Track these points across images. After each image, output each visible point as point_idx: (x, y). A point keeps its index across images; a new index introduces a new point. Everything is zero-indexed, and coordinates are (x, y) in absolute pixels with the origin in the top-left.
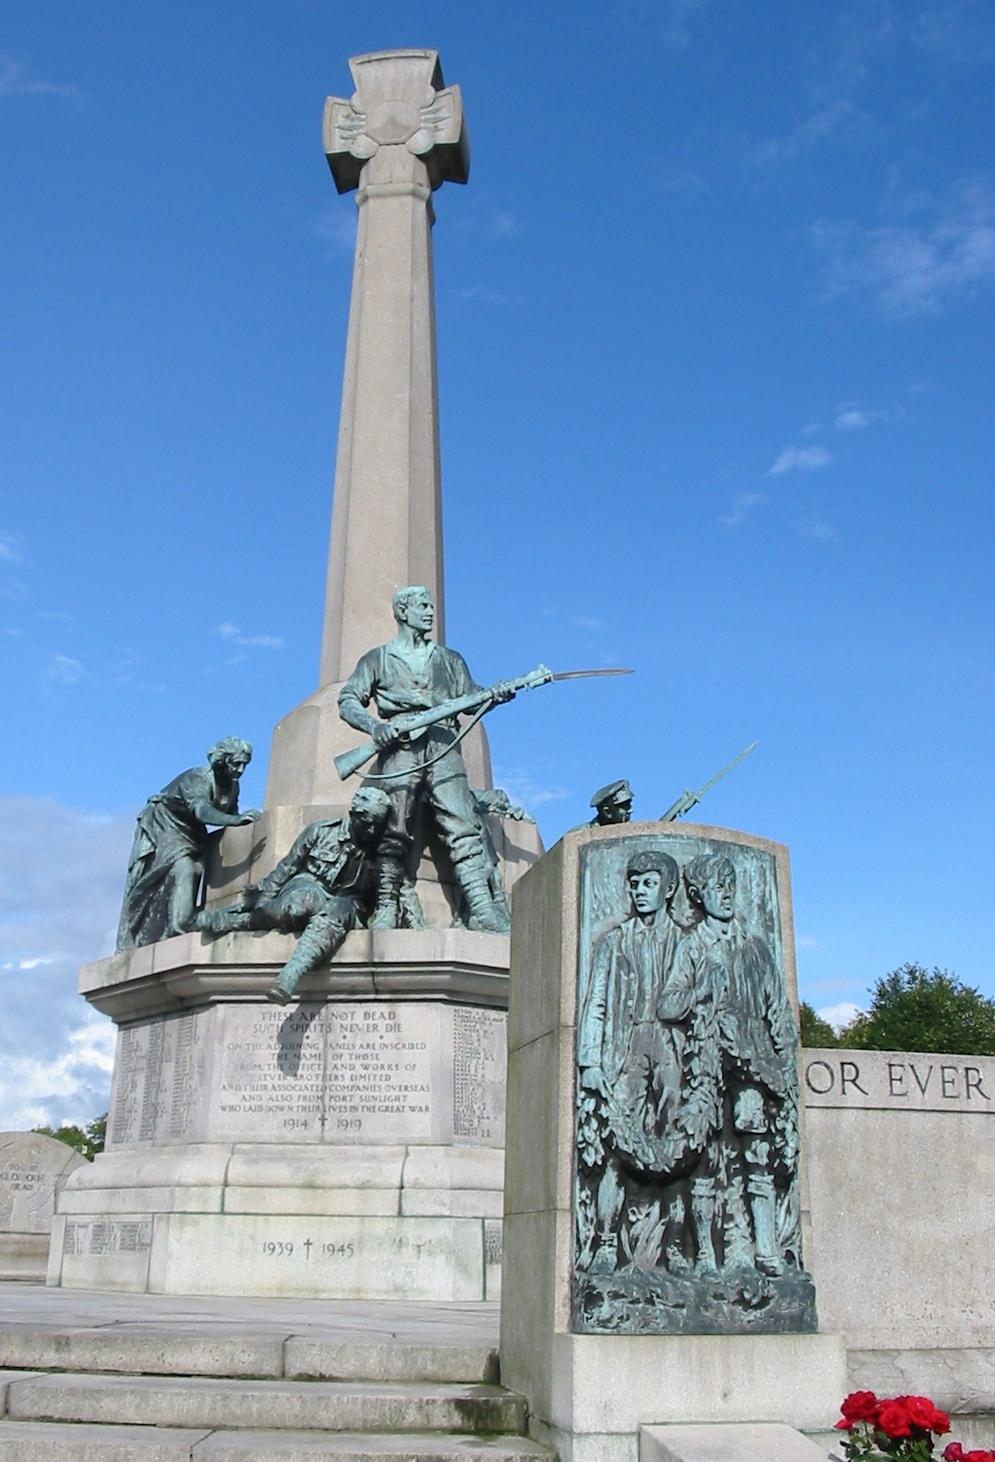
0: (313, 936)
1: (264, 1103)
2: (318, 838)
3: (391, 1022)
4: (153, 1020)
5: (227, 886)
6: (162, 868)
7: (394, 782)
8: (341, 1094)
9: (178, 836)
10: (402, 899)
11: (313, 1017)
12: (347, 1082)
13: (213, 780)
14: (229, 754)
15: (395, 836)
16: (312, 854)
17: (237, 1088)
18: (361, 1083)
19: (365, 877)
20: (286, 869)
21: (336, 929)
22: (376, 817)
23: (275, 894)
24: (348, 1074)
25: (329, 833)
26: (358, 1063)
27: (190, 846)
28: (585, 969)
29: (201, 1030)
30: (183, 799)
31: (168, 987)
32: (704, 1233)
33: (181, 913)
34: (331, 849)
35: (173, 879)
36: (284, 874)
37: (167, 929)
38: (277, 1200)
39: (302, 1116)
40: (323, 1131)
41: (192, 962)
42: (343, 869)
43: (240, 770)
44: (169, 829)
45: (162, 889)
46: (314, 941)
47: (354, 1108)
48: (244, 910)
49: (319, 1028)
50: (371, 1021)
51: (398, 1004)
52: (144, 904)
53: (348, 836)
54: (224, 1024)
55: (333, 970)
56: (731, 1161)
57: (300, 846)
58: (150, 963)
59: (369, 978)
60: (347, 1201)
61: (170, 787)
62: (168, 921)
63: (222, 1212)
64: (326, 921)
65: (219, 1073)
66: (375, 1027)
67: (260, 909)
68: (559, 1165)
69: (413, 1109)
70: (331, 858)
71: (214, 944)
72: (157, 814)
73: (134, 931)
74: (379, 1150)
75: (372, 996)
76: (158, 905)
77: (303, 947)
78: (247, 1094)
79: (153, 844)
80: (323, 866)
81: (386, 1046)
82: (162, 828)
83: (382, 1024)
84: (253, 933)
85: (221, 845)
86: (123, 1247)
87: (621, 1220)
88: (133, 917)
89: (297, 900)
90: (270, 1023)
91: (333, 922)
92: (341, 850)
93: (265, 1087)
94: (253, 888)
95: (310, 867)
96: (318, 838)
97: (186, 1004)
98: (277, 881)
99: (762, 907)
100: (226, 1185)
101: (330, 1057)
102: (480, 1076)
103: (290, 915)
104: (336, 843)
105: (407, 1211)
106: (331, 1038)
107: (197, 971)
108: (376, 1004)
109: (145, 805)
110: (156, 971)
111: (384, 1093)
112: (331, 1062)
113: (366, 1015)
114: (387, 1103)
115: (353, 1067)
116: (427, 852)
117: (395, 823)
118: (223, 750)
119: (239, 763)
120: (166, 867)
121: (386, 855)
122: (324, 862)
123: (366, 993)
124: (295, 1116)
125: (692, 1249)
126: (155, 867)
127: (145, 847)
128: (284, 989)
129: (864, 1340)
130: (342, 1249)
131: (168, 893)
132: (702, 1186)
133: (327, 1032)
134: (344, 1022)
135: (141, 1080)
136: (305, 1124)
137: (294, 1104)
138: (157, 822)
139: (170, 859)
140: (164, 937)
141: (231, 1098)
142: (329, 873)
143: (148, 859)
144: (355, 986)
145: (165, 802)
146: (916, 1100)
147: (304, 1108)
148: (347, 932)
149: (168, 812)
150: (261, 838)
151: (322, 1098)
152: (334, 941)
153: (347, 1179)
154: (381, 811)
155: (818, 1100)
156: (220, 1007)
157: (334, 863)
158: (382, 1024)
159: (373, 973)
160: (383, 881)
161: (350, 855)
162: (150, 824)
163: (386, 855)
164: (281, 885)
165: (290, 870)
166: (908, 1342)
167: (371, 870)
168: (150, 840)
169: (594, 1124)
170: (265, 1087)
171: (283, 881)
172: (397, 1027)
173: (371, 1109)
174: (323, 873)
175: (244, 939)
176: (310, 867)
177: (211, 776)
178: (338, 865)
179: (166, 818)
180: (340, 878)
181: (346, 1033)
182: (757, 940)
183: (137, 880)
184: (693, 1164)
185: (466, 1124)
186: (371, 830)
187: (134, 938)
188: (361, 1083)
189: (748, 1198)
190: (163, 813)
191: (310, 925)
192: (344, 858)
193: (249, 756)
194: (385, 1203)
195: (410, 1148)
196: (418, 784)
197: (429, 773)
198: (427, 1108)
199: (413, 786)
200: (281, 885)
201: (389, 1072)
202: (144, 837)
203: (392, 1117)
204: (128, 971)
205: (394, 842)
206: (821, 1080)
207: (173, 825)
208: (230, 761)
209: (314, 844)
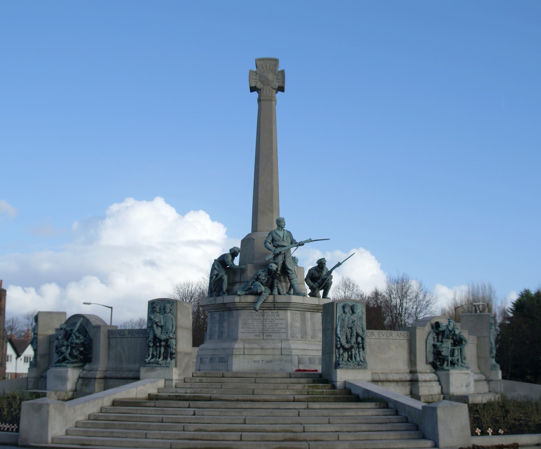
1: (250, 331)
8: (267, 329)
10: (278, 287)
12: (268, 327)
17: (244, 328)
18: (271, 327)
24: (268, 325)
26: (270, 323)
28: (337, 320)
32: (353, 356)
38: (255, 352)
39: (259, 334)
40: (263, 337)
47: (270, 332)
50: (273, 314)
56: (357, 347)
60: (270, 352)
63: (244, 354)
65: (240, 326)
66: (274, 315)
68: (130, 328)
69: (282, 333)
70: (264, 278)
74: (276, 341)
78: (246, 329)
81: (276, 319)
86: (219, 362)
87: (342, 355)
92: (266, 277)
93: (250, 328)
95: (259, 280)
97: (230, 309)
99: (362, 311)
100: (244, 349)
101: (264, 322)
102: (295, 325)
105: (283, 354)
106: (264, 317)
111: (276, 329)
112: (264, 323)
113: (272, 313)
114: (277, 331)
115: (269, 324)
124: (257, 334)
125: (352, 359)
129: (374, 371)
130: (270, 362)
132: (353, 350)
135: (217, 325)
136: (259, 336)
137: (257, 331)
141: (243, 330)
143: (217, 275)
146: (382, 337)
147: (259, 332)
151: (263, 330)
153: (270, 347)
155: (368, 337)
161: (268, 277)
166: (380, 372)
168: (217, 270)
169: (339, 342)
170: (250, 328)
172: (279, 315)
173: (273, 333)
176: (259, 280)
181: (268, 317)
182: (361, 316)
184: (352, 347)
185: (293, 336)
188: (271, 327)
189: (359, 352)
192: (266, 279)
194: (278, 352)
195: (282, 341)
198: (285, 332)
201: (277, 325)
202: (215, 270)
203: (278, 334)
206: (369, 334)
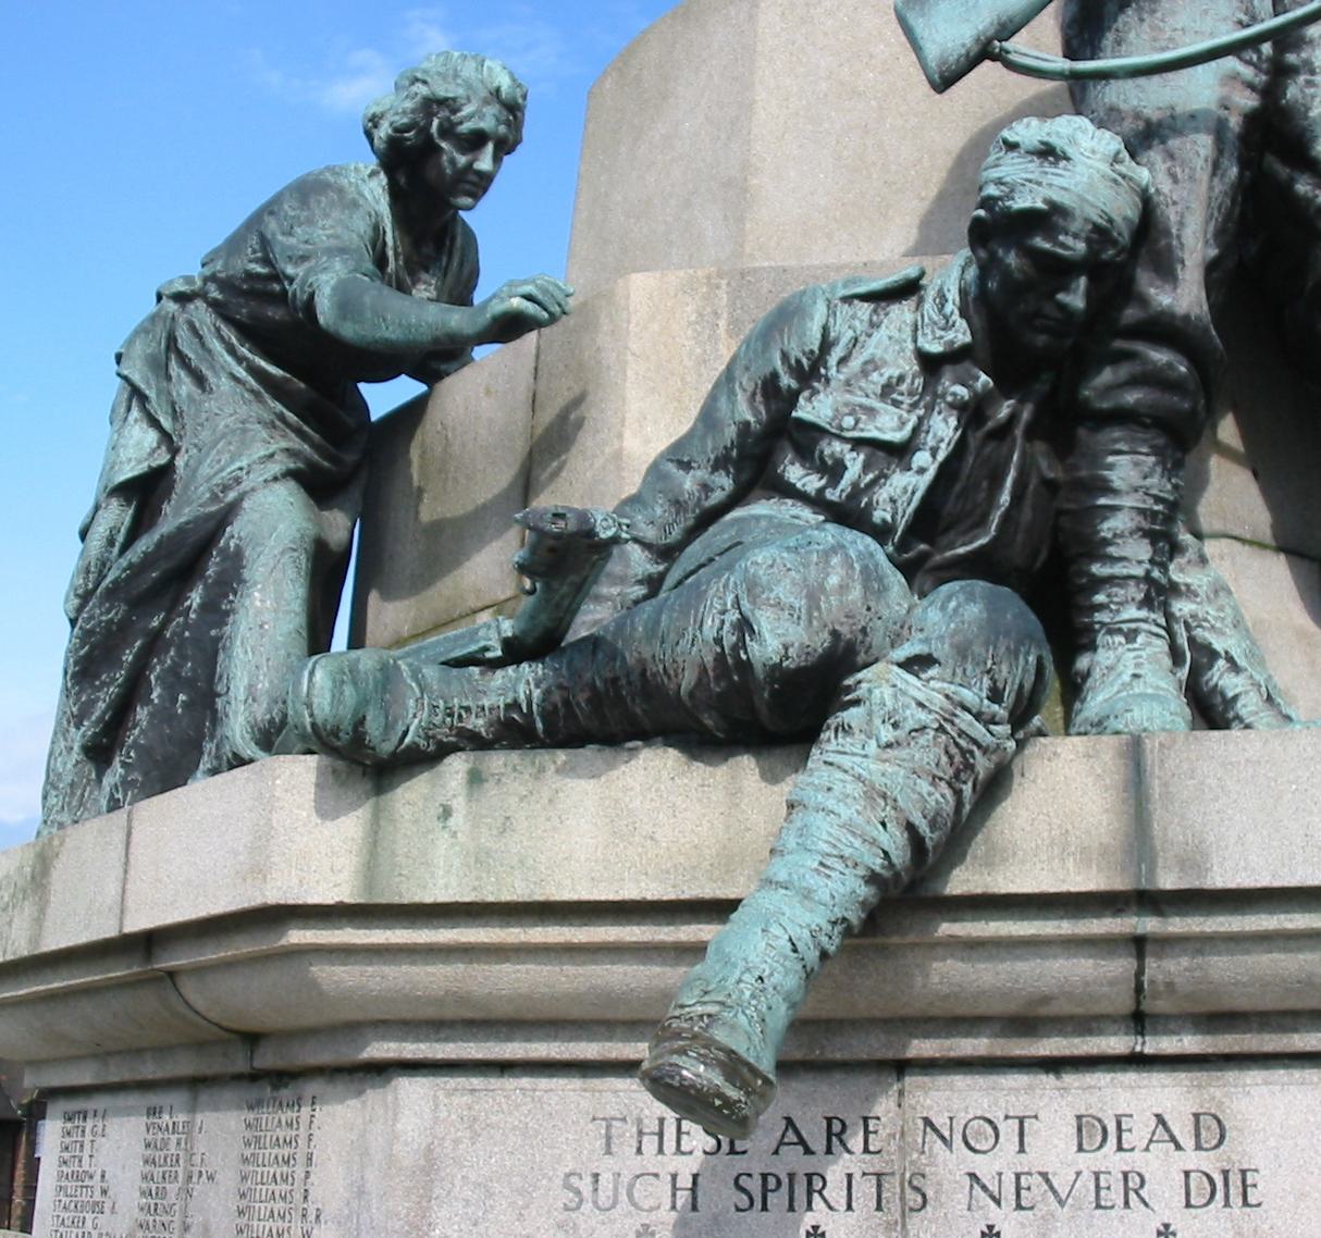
0: (873, 769)
2: (826, 345)
3: (1208, 1162)
4: (154, 1099)
5: (431, 592)
6: (196, 521)
7: (1152, 97)
9: (256, 410)
10: (1182, 607)
11: (835, 1135)
13: (383, 207)
14: (443, 102)
15: (1164, 329)
16: (804, 411)
19: (1027, 514)
20: (688, 483)
21: (978, 731)
22: (1100, 234)
23: (640, 591)
25: (874, 325)
27: (295, 443)
29: (330, 1183)
30: (277, 276)
31: (190, 989)
33: (263, 685)
34: (887, 390)
35: (236, 560)
36: (678, 504)
37: (209, 747)
41: (276, 892)
42: (948, 472)
43: (484, 163)
44: (225, 384)
45: (195, 598)
46: (877, 795)
48: (515, 652)
49: (865, 1190)
50: (1110, 1160)
51: (1231, 1076)
52: (128, 657)
53: (961, 334)
54: (429, 1166)
55: (946, 929)
57: (746, 382)
58: (113, 889)
59: (1120, 967)
61: (234, 244)
62: (216, 719)
64: (931, 689)
66: (1134, 1187)
67: (593, 643)
70: (889, 426)
71: (376, 818)
72: (183, 334)
73: (99, 752)
75: (1117, 1044)
76: (183, 657)
77: (820, 823)
79: (166, 437)
80: (855, 463)
82: (200, 380)
83: (1163, 1169)
84: (561, 756)
85: (415, 453)
88: (92, 703)
89: (784, 591)
90: (635, 1164)
91: (968, 696)
92: (929, 395)
94: (572, 525)
95: (795, 473)
96: (826, 345)
97: (267, 1059)
98: (650, 534)
103: (746, 667)
104: (910, 366)
107: (298, 936)
108: (1130, 1077)
109: (151, 306)
110: (137, 923)
113: (1089, 1131)
116: (1228, 430)
117: (1166, 269)
118: (422, 90)
119: (476, 141)
120: (209, 516)
121: (1122, 417)
122: (858, 444)
123: (1087, 1024)
126: (174, 516)
127: (139, 449)
128: (740, 1046)
131: (217, 612)
133: (907, 1211)
134: (984, 1166)
138: (184, 362)
139: (225, 488)
140: (199, 774)
142: (883, 494)
144: (1046, 999)
145: (215, 294)
148: (1021, 745)
149: (226, 331)
150: (560, 402)
152: (967, 789)
154: (1123, 209)
156: (411, 1089)
157: (900, 453)
158: (1163, 1169)
159: (1139, 945)
160: (1107, 528)
161: (972, 414)
162: (160, 369)
163: (1122, 417)
164: (667, 553)
165: (706, 488)
167: (1051, 486)
168: (154, 423)
171: (676, 533)
174: (857, 491)
175: (516, 786)
176: (795, 473)
177: (375, 193)
178: (921, 458)
179: (217, 346)
180: (930, 518)
183: (103, 565)
186: (1075, 298)
187: (99, 780)
190: (204, 331)
191: (852, 716)
192: (944, 428)
193: (513, 110)
196: (1251, 118)
197: (1292, 71)
199: (1235, 122)
200: (667, 553)
202: (135, 413)
204: (39, 920)
205: (1160, 356)
207: (241, 372)
208: (448, 131)
209: (810, 373)
